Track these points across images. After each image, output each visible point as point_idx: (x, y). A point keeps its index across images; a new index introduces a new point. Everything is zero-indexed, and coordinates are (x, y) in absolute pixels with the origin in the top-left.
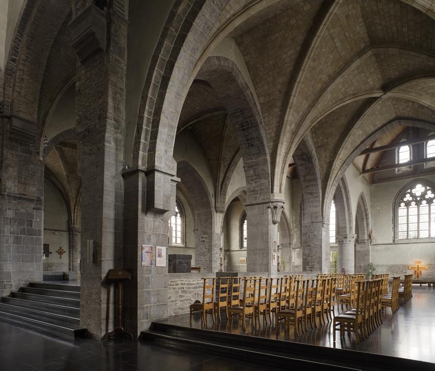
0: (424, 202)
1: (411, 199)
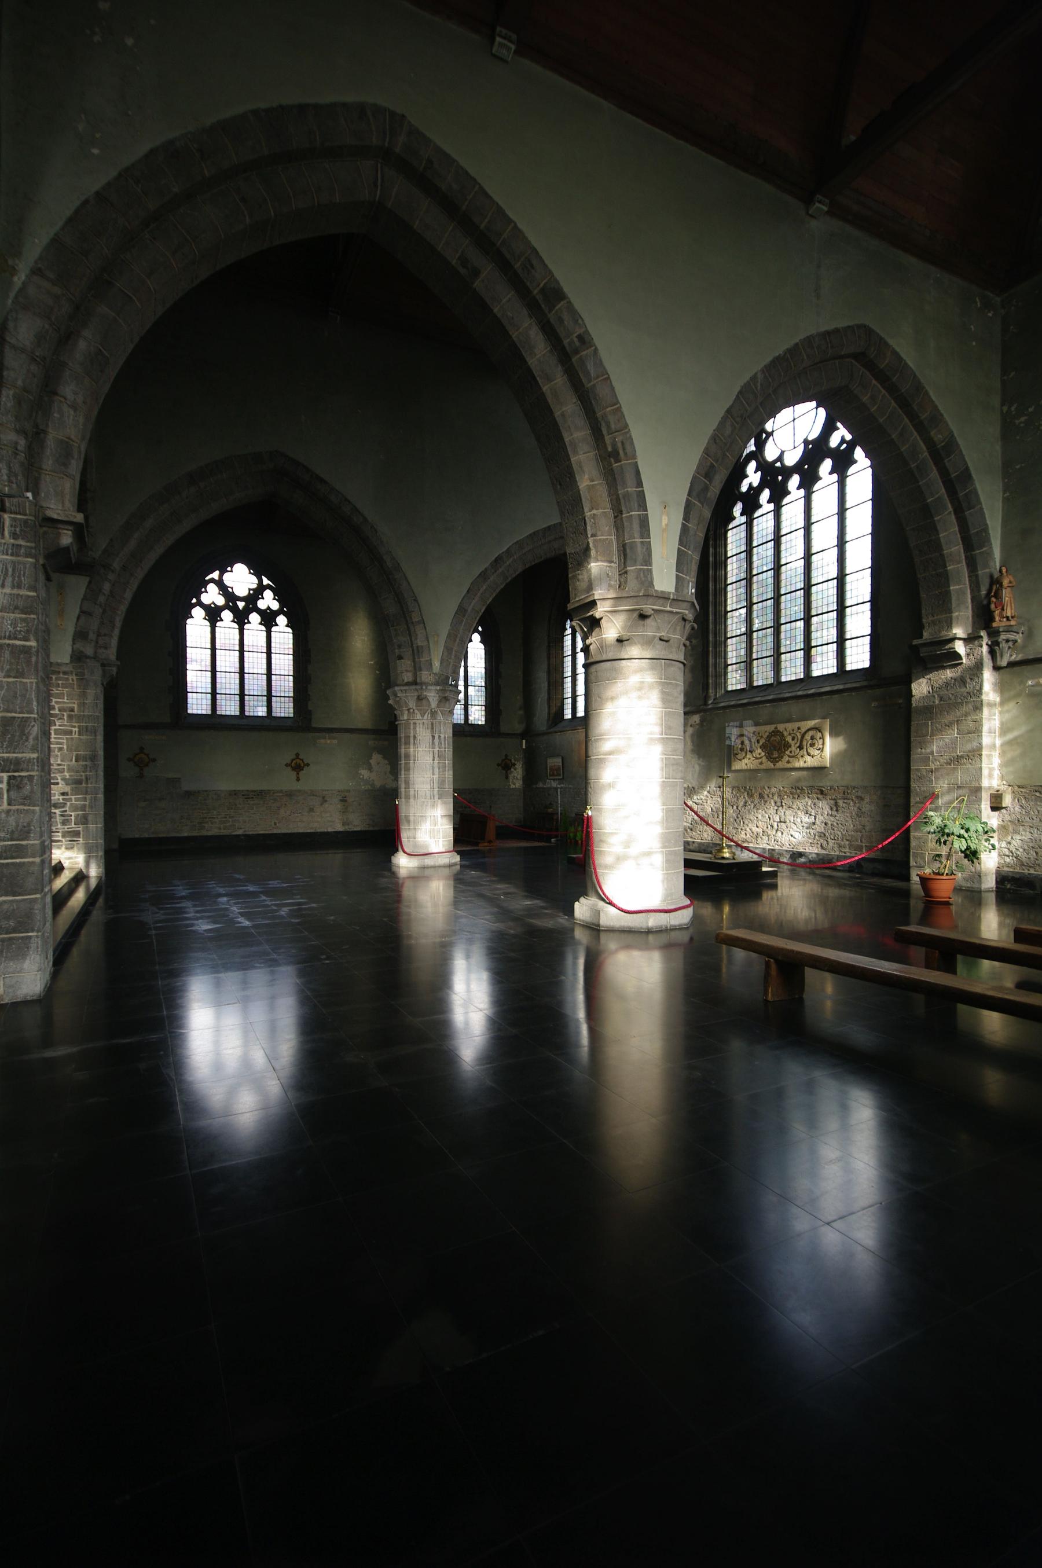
0: (255, 618)
1: (220, 601)
